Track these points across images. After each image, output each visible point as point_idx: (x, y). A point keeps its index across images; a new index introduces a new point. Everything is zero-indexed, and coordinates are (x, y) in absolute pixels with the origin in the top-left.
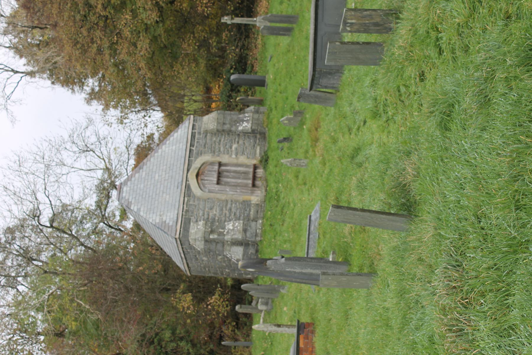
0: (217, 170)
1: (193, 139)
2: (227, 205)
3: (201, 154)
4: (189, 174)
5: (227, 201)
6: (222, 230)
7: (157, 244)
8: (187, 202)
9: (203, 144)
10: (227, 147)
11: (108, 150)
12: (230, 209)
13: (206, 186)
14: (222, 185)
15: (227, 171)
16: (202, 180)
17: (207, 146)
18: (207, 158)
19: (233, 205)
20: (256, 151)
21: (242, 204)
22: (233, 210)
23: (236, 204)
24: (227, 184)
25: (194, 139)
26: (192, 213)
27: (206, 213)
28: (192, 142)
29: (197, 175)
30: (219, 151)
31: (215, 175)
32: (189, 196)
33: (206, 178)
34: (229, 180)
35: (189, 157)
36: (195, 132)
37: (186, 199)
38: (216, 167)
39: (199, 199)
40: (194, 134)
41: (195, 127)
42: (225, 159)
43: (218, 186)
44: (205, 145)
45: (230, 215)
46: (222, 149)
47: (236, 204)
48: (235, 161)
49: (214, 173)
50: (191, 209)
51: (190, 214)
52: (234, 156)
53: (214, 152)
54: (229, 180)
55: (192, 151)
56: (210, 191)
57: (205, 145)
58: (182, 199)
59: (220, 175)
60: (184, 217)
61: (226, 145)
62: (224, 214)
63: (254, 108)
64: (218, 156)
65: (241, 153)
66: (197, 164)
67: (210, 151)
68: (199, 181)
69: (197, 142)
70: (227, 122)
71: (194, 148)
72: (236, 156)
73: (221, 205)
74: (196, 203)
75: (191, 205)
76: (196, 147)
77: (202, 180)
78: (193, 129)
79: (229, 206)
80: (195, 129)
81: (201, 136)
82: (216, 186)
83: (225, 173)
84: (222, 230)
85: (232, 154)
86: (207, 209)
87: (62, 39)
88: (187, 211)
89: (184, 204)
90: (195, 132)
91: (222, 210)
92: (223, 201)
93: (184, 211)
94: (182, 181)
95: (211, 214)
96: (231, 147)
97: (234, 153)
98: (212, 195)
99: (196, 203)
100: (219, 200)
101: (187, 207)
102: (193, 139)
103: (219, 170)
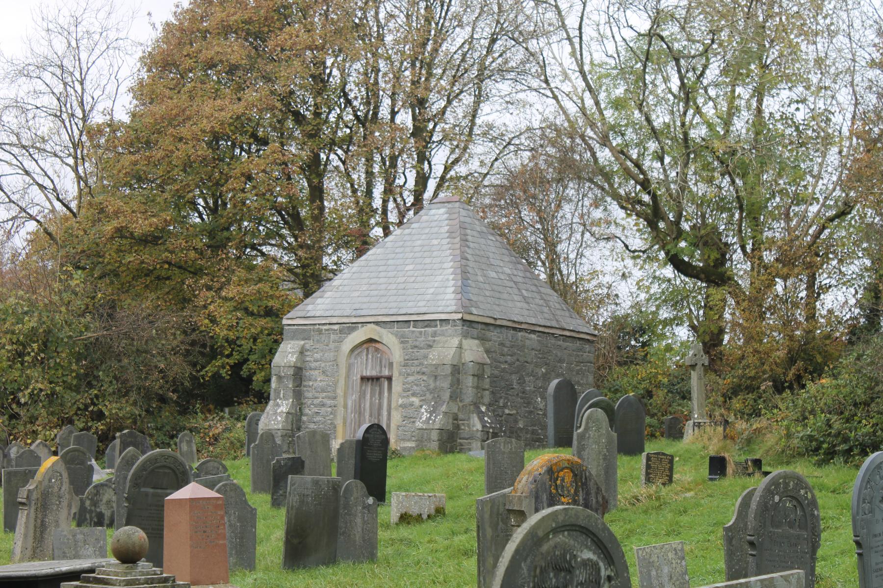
0: (383, 374)
1: (426, 323)
2: (329, 398)
3: (402, 342)
4: (372, 326)
5: (335, 398)
6: (282, 396)
7: (315, 292)
8: (332, 330)
9: (417, 344)
10: (415, 388)
11: (630, 187)
12: (323, 405)
13: (359, 359)
14: (361, 387)
15: (381, 393)
16: (368, 349)
17: (415, 350)
18: (396, 353)
19: (329, 409)
20: (409, 440)
21: (331, 424)
22: (323, 410)
23: (331, 413)
24: (362, 395)
25: (426, 327)
26: (318, 341)
27: (317, 364)
28: (419, 323)
29: (371, 340)
30: (408, 375)
31: (374, 373)
32: (341, 331)
33: (370, 356)
34: (368, 396)
35: (398, 322)
36: (436, 326)
37: (336, 327)
38: (386, 373)
39: (337, 350)
40: (433, 323)
41: (444, 324)
42: (397, 386)
43: (359, 381)
44: (416, 347)
45: (316, 406)
46: (411, 379)
47: (331, 413)
48: (393, 405)
49: (378, 368)
50: (323, 337)
51: (316, 338)
52: (400, 401)
53: (405, 365)
54: (368, 396)
55: (406, 325)
56: (350, 367)
57: (416, 347)
58: (334, 320)
59: (374, 380)
60: (312, 327)
61: (417, 385)
62: (317, 395)
63: (477, 430)
64: (400, 374)
65: (404, 414)
66: (388, 338)
67: (407, 357)
68: (365, 346)
69: (421, 333)
70: (438, 383)
71: (411, 329)
72: (401, 406)
73: (329, 389)
74: (332, 346)
75: (329, 337)
76: (413, 332)
77: (368, 349)
78: (440, 320)
79: (329, 402)
80: (441, 325)
81: (430, 338)
82: (359, 377)
83: (377, 389)
84: (282, 396)
85: (404, 397)
86: (323, 365)
87: (395, 40)
88: (320, 332)
89: (330, 324)
90: (436, 326)
91: (323, 391)
92: (334, 391)
93: (321, 327)
94: (564, 329)
95: (317, 372)
96: (413, 395)
97: (405, 401)
98: (343, 371)
99: (332, 346)
100: (336, 384)
101: (326, 330)
102: (426, 323)
103: (382, 377)
